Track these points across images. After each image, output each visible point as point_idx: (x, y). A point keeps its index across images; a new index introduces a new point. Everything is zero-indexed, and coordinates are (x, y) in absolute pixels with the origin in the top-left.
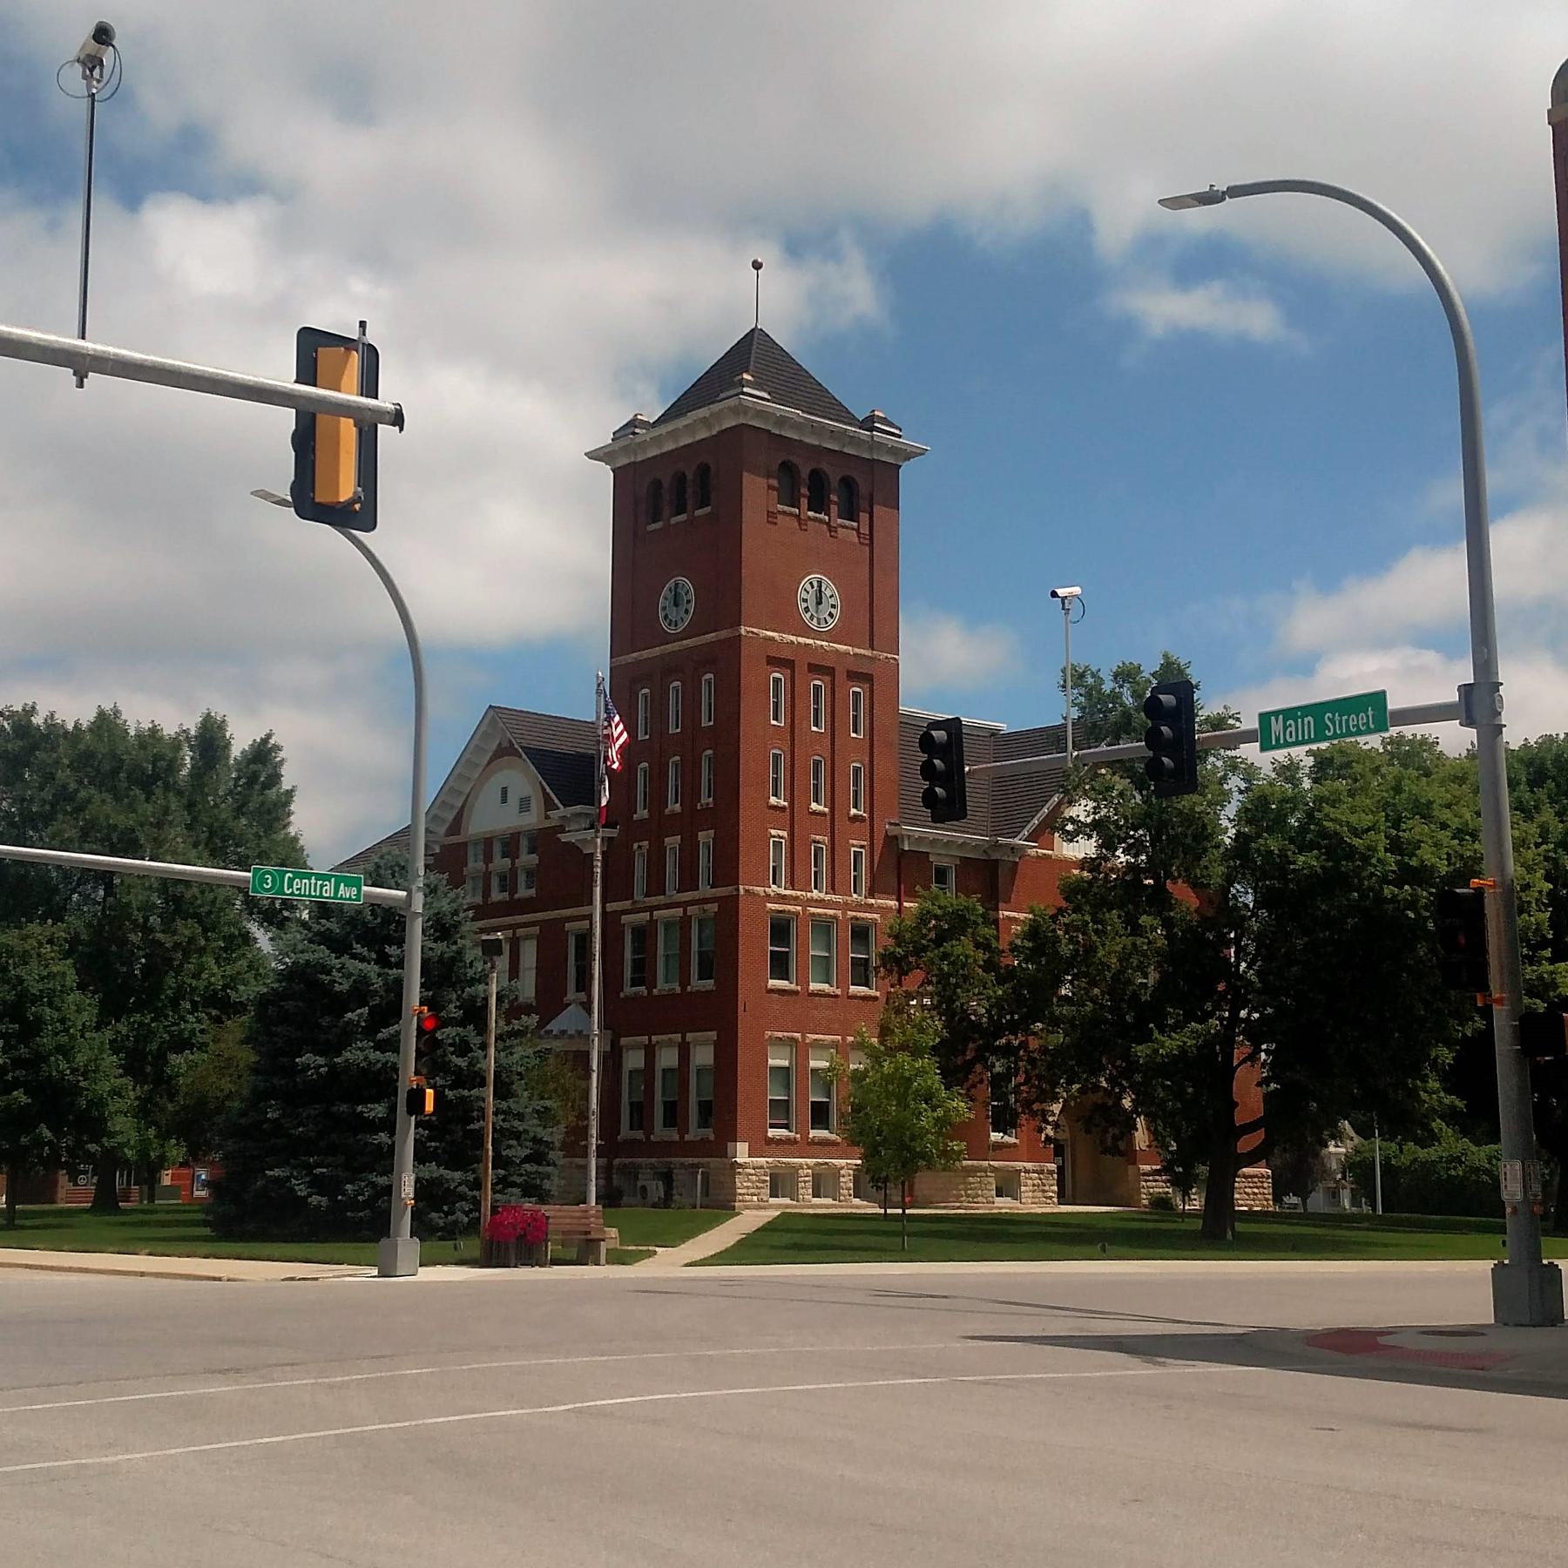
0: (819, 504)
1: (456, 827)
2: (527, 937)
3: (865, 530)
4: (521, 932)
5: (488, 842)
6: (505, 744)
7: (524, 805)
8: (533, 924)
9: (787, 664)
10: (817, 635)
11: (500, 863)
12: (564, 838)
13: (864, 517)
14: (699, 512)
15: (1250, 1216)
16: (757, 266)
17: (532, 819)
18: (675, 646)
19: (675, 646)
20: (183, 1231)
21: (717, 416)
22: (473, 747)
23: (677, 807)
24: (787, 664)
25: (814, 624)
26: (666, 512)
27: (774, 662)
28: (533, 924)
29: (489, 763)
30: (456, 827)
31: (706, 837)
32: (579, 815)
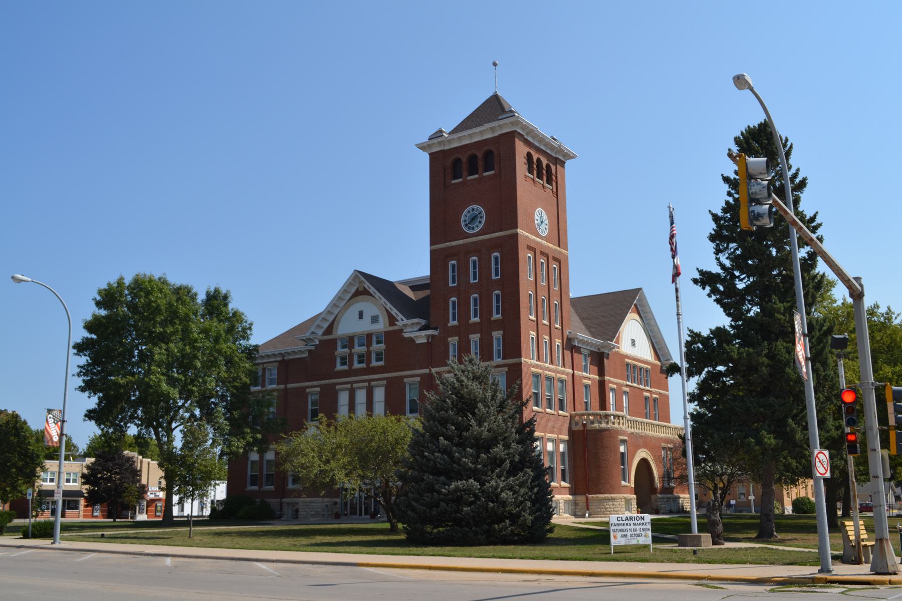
0: (540, 176)
1: (329, 330)
2: (378, 386)
3: (555, 190)
4: (373, 383)
5: (351, 339)
6: (361, 289)
7: (375, 319)
8: (417, 376)
9: (533, 250)
10: (541, 237)
11: (358, 349)
12: (406, 335)
13: (554, 184)
14: (486, 174)
15: (176, 517)
16: (495, 64)
17: (382, 326)
18: (474, 239)
19: (474, 239)
20: (327, 539)
21: (500, 126)
22: (344, 291)
23: (499, 316)
24: (533, 250)
25: (540, 232)
26: (465, 173)
27: (530, 248)
28: (417, 376)
29: (351, 299)
30: (329, 330)
31: (497, 334)
32: (413, 324)
